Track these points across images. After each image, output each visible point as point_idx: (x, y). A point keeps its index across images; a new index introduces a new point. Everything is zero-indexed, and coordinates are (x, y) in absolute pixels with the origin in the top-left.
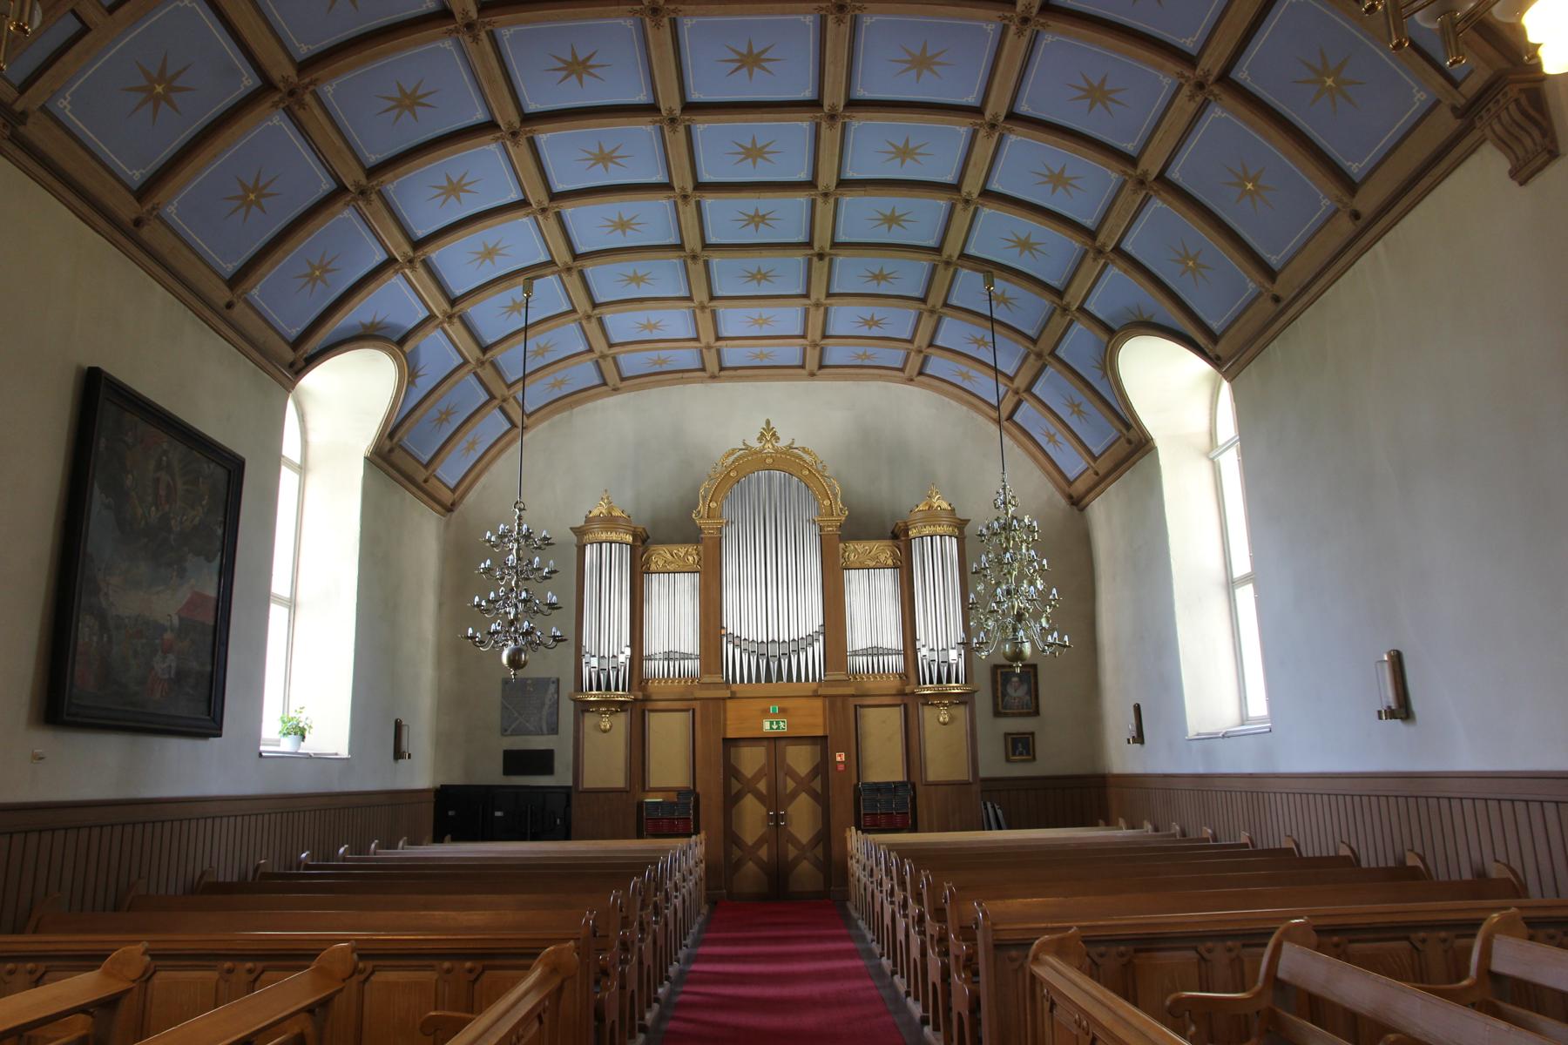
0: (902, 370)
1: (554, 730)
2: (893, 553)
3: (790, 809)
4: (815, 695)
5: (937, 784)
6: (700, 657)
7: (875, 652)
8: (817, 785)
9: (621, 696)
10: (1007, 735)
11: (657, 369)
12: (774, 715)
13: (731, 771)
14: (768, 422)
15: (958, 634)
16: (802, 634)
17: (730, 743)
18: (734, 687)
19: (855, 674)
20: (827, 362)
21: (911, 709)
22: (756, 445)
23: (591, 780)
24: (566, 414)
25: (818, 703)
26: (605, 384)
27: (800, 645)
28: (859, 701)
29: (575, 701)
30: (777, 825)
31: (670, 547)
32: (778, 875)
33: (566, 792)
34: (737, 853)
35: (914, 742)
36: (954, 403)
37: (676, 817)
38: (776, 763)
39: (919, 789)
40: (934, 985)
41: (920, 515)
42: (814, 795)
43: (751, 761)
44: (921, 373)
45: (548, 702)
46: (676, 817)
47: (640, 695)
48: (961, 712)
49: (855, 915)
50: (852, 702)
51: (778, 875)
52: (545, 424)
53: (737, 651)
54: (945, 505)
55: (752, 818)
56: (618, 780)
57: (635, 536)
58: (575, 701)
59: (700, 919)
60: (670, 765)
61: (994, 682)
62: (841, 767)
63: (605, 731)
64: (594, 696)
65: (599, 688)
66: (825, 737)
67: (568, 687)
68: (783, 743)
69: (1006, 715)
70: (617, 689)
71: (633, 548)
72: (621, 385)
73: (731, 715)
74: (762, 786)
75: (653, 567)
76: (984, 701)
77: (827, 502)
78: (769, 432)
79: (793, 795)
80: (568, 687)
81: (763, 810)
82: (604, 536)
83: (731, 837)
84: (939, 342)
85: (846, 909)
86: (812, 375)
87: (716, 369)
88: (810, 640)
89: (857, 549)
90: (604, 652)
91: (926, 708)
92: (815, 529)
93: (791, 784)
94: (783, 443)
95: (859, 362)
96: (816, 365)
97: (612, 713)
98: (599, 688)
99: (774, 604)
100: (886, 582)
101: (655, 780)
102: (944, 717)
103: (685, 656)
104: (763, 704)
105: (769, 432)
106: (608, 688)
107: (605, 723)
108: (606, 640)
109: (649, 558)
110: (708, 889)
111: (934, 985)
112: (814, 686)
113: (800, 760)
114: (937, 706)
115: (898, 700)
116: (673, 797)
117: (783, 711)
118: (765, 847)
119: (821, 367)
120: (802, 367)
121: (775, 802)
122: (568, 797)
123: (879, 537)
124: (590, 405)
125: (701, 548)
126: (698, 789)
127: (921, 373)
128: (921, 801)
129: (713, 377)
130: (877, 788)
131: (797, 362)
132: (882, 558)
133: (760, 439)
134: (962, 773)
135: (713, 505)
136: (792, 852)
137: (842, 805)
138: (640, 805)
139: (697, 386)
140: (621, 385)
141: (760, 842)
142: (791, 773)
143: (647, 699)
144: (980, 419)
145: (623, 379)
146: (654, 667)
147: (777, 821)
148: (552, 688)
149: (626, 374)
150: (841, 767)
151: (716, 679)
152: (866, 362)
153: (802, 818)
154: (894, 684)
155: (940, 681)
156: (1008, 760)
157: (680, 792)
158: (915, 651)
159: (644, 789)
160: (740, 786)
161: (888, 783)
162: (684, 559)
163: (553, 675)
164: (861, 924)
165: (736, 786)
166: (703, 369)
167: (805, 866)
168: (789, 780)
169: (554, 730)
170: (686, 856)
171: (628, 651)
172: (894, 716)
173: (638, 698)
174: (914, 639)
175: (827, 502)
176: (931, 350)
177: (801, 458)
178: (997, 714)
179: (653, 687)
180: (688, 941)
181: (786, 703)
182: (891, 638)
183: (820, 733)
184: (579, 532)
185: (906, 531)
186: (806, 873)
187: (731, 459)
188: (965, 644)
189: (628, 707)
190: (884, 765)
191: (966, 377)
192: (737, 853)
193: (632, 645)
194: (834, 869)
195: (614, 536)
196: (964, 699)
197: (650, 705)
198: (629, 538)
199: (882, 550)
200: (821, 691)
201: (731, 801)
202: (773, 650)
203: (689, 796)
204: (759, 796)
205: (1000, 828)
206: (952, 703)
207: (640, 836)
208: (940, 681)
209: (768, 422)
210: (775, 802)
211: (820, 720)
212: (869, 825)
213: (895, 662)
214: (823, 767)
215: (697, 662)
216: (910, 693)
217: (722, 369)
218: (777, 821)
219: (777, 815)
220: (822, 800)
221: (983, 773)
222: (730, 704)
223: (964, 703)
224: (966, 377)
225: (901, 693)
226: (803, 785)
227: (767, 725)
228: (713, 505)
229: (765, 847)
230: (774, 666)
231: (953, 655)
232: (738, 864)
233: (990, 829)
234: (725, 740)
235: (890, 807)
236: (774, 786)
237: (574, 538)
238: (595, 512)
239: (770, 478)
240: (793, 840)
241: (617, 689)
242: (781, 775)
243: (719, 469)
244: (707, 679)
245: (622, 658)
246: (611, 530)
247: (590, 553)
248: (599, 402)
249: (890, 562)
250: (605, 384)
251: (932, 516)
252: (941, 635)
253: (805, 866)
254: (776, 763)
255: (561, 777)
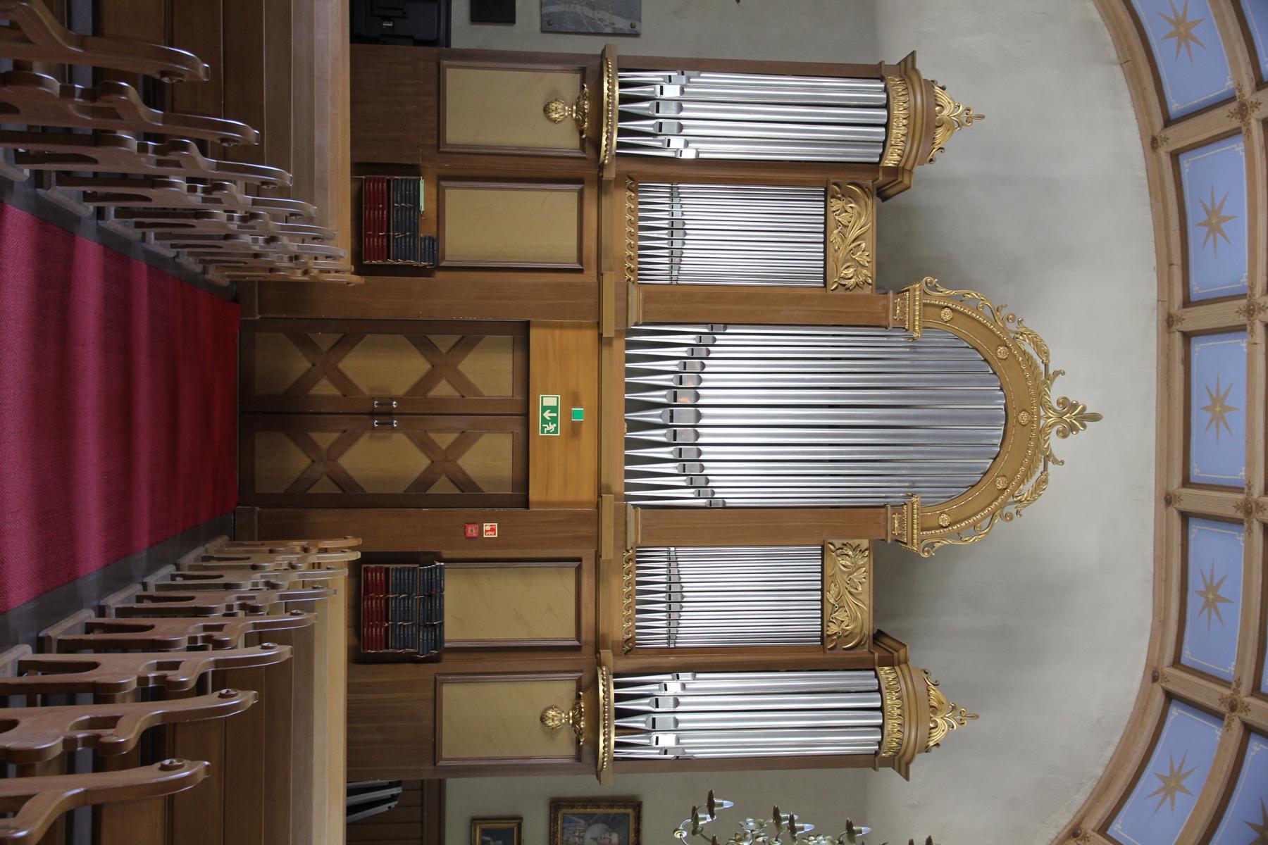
0: (1177, 662)
1: (549, 26)
2: (851, 635)
3: (400, 439)
4: (601, 489)
5: (436, 700)
6: (674, 285)
7: (674, 598)
8: (443, 487)
9: (610, 139)
10: (519, 820)
11: (1195, 216)
12: (568, 414)
13: (470, 334)
14: (1095, 417)
15: (702, 747)
16: (710, 469)
17: (521, 333)
18: (619, 344)
19: (639, 558)
20: (1195, 528)
21: (568, 656)
22: (1055, 394)
23: (458, 80)
24: (1112, 53)
25: (586, 493)
26: (1168, 122)
27: (690, 462)
28: (588, 566)
29: (603, 56)
30: (373, 414)
31: (871, 236)
32: (287, 413)
33: (438, 39)
34: (325, 341)
35: (489, 664)
36: (1110, 751)
37: (388, 227)
38: (479, 415)
39: (429, 670)
40: (94, 665)
41: (920, 687)
42: (424, 482)
43: (489, 371)
44: (1170, 697)
45: (598, 15)
46: (388, 227)
47: (609, 174)
48: (563, 748)
49: (189, 559)
50: (587, 554)
51: (287, 413)
52: (1095, 15)
53: (681, 351)
54: (938, 736)
55: (387, 370)
56: (458, 132)
57: (895, 171)
58: (603, 56)
59: (189, 262)
60: (484, 226)
61: (612, 801)
62: (472, 531)
63: (546, 110)
64: (611, 90)
65: (624, 99)
66: (526, 504)
67: (625, 47)
68: (519, 429)
69: (553, 820)
70: (622, 132)
71: (874, 167)
72: (1163, 152)
73: (570, 336)
74: (443, 389)
75: (835, 204)
76: (581, 785)
77: (944, 520)
78: (1076, 418)
79: (425, 445)
80: (625, 47)
81: (401, 391)
82: (899, 112)
83: (353, 332)
84: (1175, 712)
85: (211, 535)
86: (1169, 500)
87: (1188, 326)
88: (699, 482)
89: (854, 570)
90: (690, 110)
91: (572, 686)
92: (897, 496)
93: (445, 440)
94: (1055, 443)
95: (1195, 583)
96: (1185, 508)
97: (579, 123)
98: (624, 99)
99: (749, 420)
100: (800, 620)
101: (459, 199)
102: (556, 718)
103: (675, 257)
104: (589, 396)
105: (1076, 418)
106: (624, 116)
107: (561, 111)
108: (706, 116)
109: (854, 198)
110: (262, 284)
111: (94, 665)
112: (618, 487)
113: (488, 459)
114: (577, 707)
115: (587, 635)
116: (427, 230)
117: (574, 430)
118: (335, 392)
119: (1185, 517)
120: (1186, 482)
121: (411, 412)
122: (433, 43)
123: (879, 610)
124: (1126, 97)
125: (868, 290)
126: (440, 275)
127: (1170, 697)
128: (407, 672)
129: (1170, 321)
130: (433, 594)
131: (1196, 473)
132: (840, 615)
133: (1064, 402)
134: (453, 747)
135: (946, 315)
136: (325, 439)
137: (398, 532)
138: (414, 170)
139: (1149, 292)
140: (1163, 152)
141: (461, 383)
142: (465, 441)
143: (601, 187)
144: (1080, 799)
145: (1175, 156)
146: (658, 204)
147: (381, 414)
148: (622, 24)
149: (1186, 163)
150: (472, 531)
151: (635, 313)
152: (1194, 603)
153: (383, 458)
154: (617, 627)
155: (621, 714)
156: (474, 821)
157: (435, 244)
158: (675, 671)
159: (442, 178)
160: (444, 351)
161: (440, 614)
162: (850, 261)
163: (645, 26)
164: (163, 574)
165: (444, 343)
166: (1187, 303)
167: (299, 462)
168: (452, 437)
169: (549, 26)
170: (323, 244)
171: (689, 154)
172: (560, 630)
173: (603, 167)
174: (695, 669)
175: (944, 520)
176: (1237, 729)
177: (1027, 476)
178: (556, 805)
179: (621, 201)
180: (112, 222)
181: (588, 436)
182: (700, 624)
183: (534, 496)
184: (907, 68)
185: (890, 662)
186: (284, 462)
187: (1030, 350)
188: (683, 764)
189: (590, 153)
190: (476, 607)
191: (1171, 785)
192: (325, 341)
193: (699, 162)
194: (288, 516)
195: (898, 131)
196: (585, 752)
197: (591, 195)
198: (891, 161)
199: (854, 616)
200: (608, 502)
201: (419, 333)
202: (684, 416)
203: (427, 258)
204: (427, 381)
205: (350, 810)
206: (579, 733)
207: (358, 167)
208: (621, 714)
209: (1095, 417)
210: (411, 412)
211: (556, 495)
212: (367, 582)
213: (655, 631)
214: (472, 497)
215: (665, 280)
216: (599, 662)
217: (1187, 337)
218: (381, 414)
219: (390, 414)
220: (416, 496)
221: (454, 787)
222: (589, 336)
223: (578, 758)
224: (1171, 785)
225: (599, 643)
226: (443, 462)
227: (550, 401)
228: (946, 315)
229: (335, 392)
230: (653, 416)
231: (667, 740)
232: (305, 344)
233: (350, 792)
234: (527, 325)
235: (396, 623)
236: (441, 410)
237: (894, 57)
238: (944, 98)
239: (992, 419)
240: (348, 440)
241: (622, 132)
242: (463, 423)
243: (1012, 326)
244: (635, 296)
245: (677, 143)
246: (910, 135)
247: (871, 90)
248: (1130, 114)
249: (833, 629)
250: (1168, 122)
251: (920, 710)
252: (698, 718)
253: (299, 462)
254: (479, 415)
255: (464, 32)
